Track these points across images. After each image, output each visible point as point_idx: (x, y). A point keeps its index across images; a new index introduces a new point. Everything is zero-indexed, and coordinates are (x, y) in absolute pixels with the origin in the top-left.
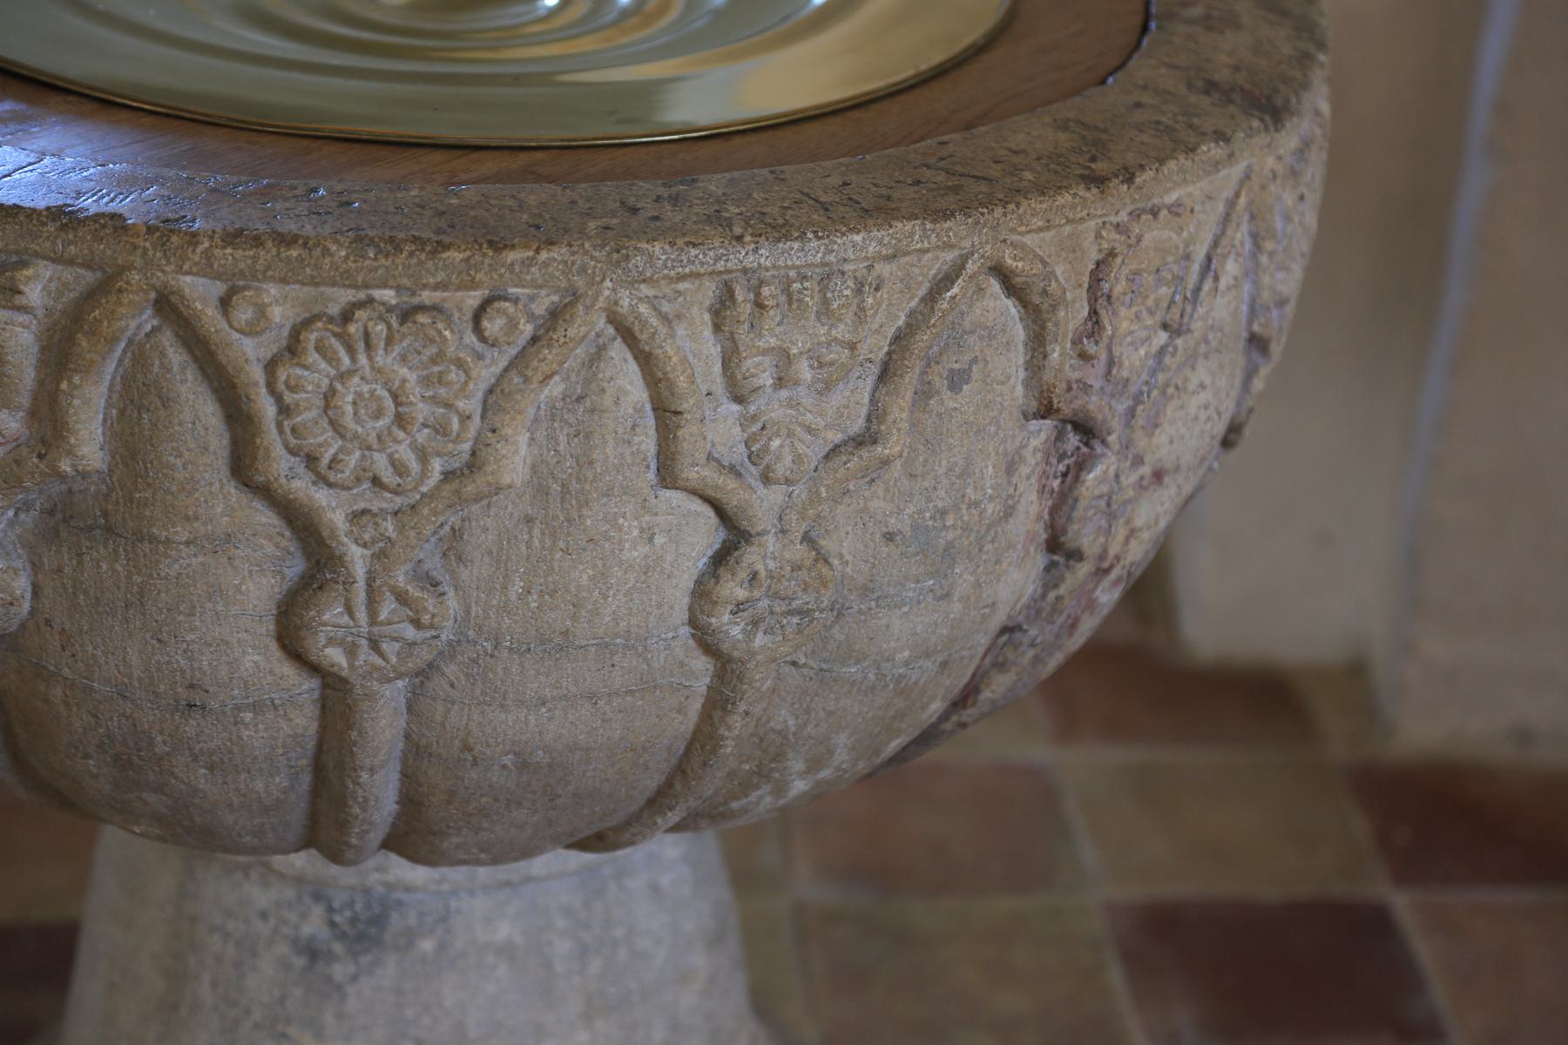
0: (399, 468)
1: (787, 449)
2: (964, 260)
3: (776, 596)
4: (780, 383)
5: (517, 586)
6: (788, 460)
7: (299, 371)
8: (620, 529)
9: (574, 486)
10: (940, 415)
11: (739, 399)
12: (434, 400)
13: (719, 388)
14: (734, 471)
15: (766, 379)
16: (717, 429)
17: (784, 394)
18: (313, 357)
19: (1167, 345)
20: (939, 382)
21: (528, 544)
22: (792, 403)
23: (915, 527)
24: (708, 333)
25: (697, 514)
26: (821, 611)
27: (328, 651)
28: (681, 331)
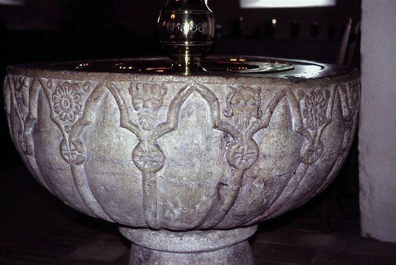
0: (71, 116)
1: (147, 122)
2: (187, 86)
3: (149, 157)
4: (144, 106)
5: (94, 145)
6: (148, 125)
7: (56, 96)
8: (112, 134)
9: (102, 124)
10: (186, 122)
11: (136, 109)
12: (76, 102)
13: (132, 106)
14: (136, 126)
15: (141, 105)
16: (134, 115)
17: (145, 109)
18: (58, 93)
19: (255, 122)
20: (186, 115)
21: (95, 136)
22: (147, 112)
23: (181, 147)
24: (128, 94)
25: (131, 136)
26: (160, 162)
27: (65, 156)
28: (122, 92)
